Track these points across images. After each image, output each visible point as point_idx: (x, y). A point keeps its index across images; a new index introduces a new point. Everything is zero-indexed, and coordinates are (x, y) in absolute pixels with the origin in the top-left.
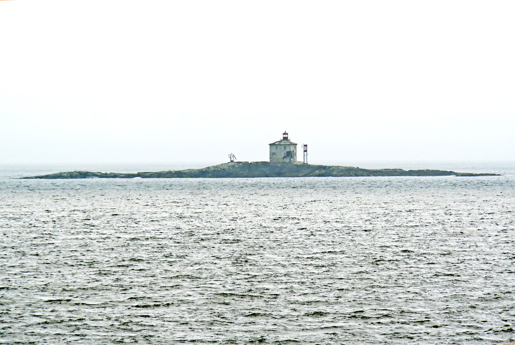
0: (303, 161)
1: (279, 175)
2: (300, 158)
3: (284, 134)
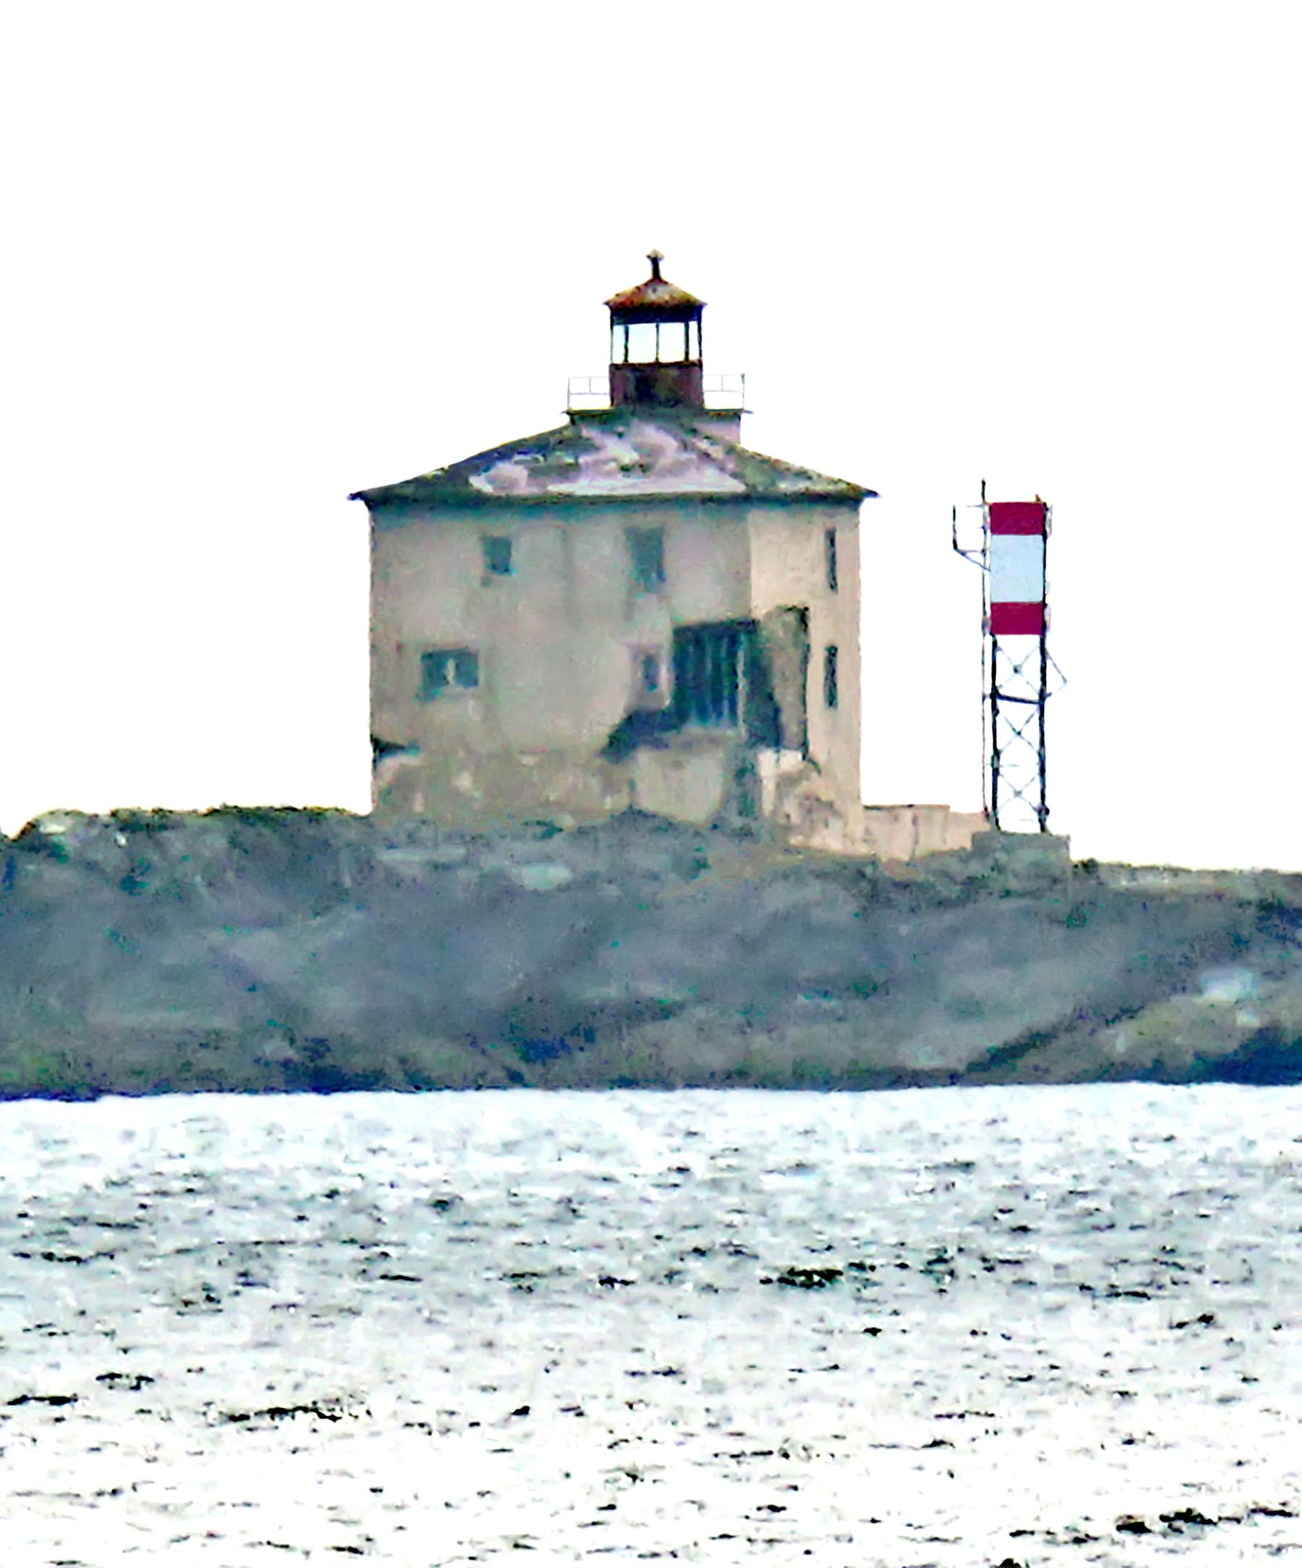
0: (971, 801)
1: (543, 1045)
2: (908, 744)
3: (627, 311)
